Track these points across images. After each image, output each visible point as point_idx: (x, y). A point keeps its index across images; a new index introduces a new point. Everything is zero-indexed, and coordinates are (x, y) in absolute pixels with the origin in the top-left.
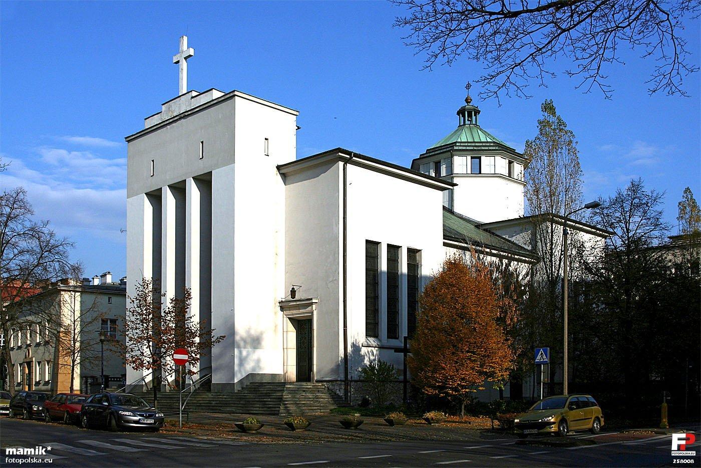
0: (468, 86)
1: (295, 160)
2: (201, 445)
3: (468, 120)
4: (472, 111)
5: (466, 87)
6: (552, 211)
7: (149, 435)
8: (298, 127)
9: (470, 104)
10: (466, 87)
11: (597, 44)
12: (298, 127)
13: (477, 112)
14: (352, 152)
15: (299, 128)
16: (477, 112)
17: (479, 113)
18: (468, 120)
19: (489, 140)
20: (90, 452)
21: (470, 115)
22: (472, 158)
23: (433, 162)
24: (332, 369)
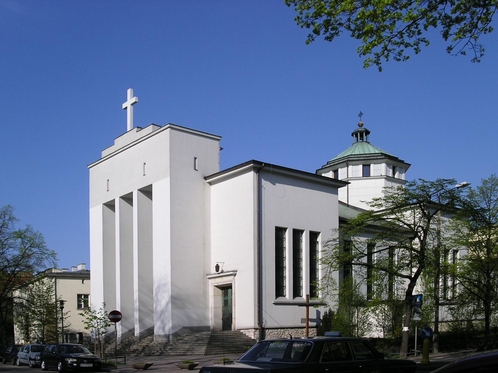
0: (361, 115)
1: (219, 171)
2: (218, 358)
3: (360, 139)
4: (363, 133)
5: (359, 116)
6: (445, 281)
7: (488, 355)
8: (221, 148)
9: (362, 127)
10: (359, 116)
11: (475, 45)
12: (221, 148)
13: (367, 133)
14: (263, 163)
15: (221, 149)
16: (367, 133)
17: (369, 134)
18: (360, 139)
19: (377, 152)
20: (181, 359)
21: (362, 136)
22: (363, 165)
23: (333, 171)
24: (223, 306)
